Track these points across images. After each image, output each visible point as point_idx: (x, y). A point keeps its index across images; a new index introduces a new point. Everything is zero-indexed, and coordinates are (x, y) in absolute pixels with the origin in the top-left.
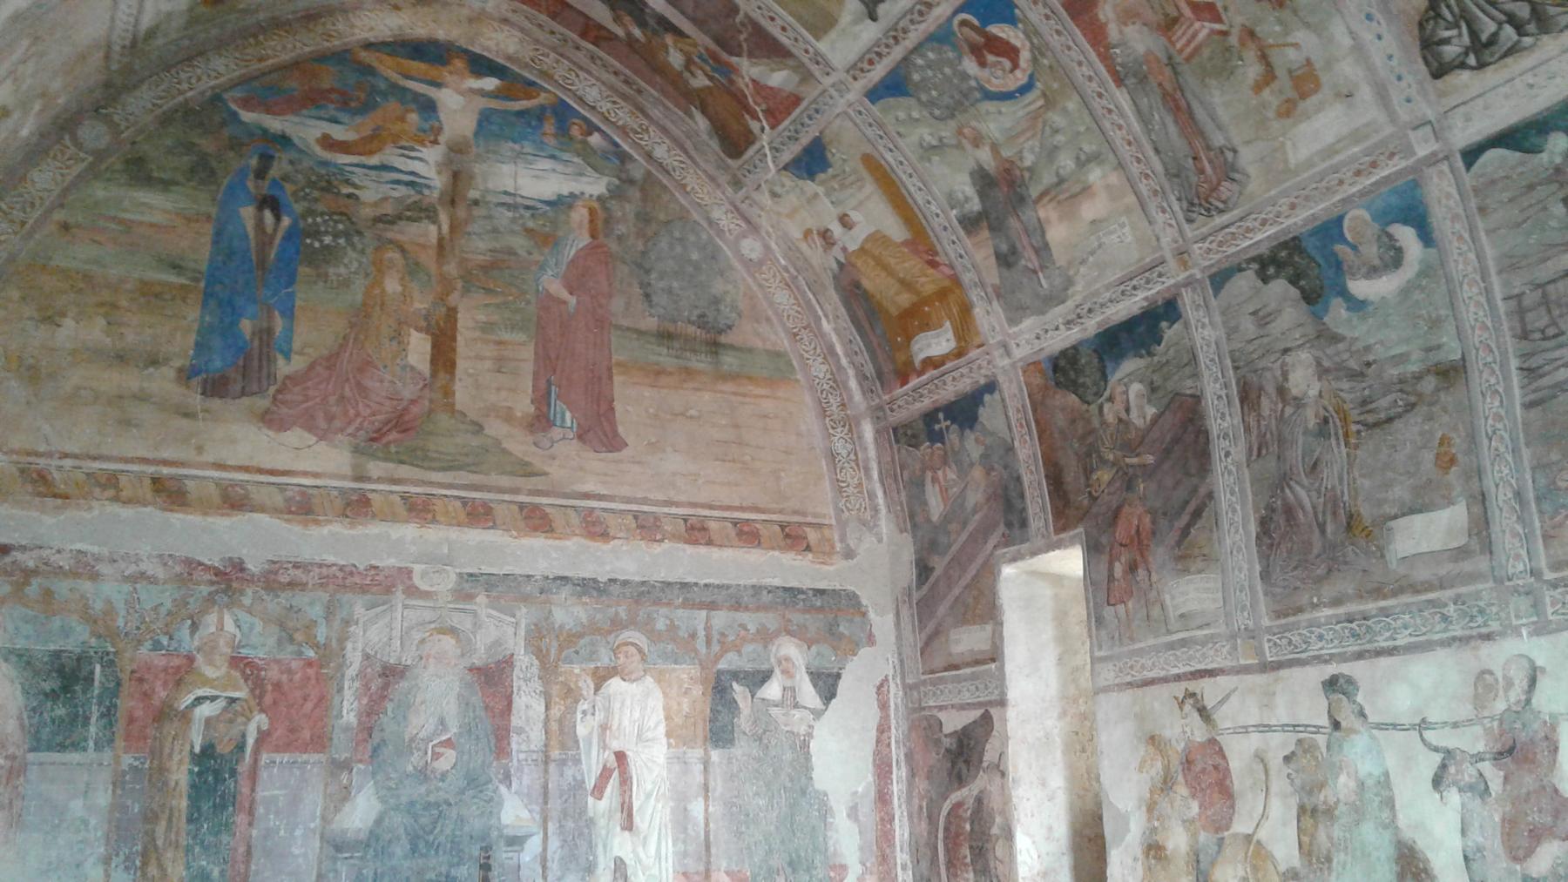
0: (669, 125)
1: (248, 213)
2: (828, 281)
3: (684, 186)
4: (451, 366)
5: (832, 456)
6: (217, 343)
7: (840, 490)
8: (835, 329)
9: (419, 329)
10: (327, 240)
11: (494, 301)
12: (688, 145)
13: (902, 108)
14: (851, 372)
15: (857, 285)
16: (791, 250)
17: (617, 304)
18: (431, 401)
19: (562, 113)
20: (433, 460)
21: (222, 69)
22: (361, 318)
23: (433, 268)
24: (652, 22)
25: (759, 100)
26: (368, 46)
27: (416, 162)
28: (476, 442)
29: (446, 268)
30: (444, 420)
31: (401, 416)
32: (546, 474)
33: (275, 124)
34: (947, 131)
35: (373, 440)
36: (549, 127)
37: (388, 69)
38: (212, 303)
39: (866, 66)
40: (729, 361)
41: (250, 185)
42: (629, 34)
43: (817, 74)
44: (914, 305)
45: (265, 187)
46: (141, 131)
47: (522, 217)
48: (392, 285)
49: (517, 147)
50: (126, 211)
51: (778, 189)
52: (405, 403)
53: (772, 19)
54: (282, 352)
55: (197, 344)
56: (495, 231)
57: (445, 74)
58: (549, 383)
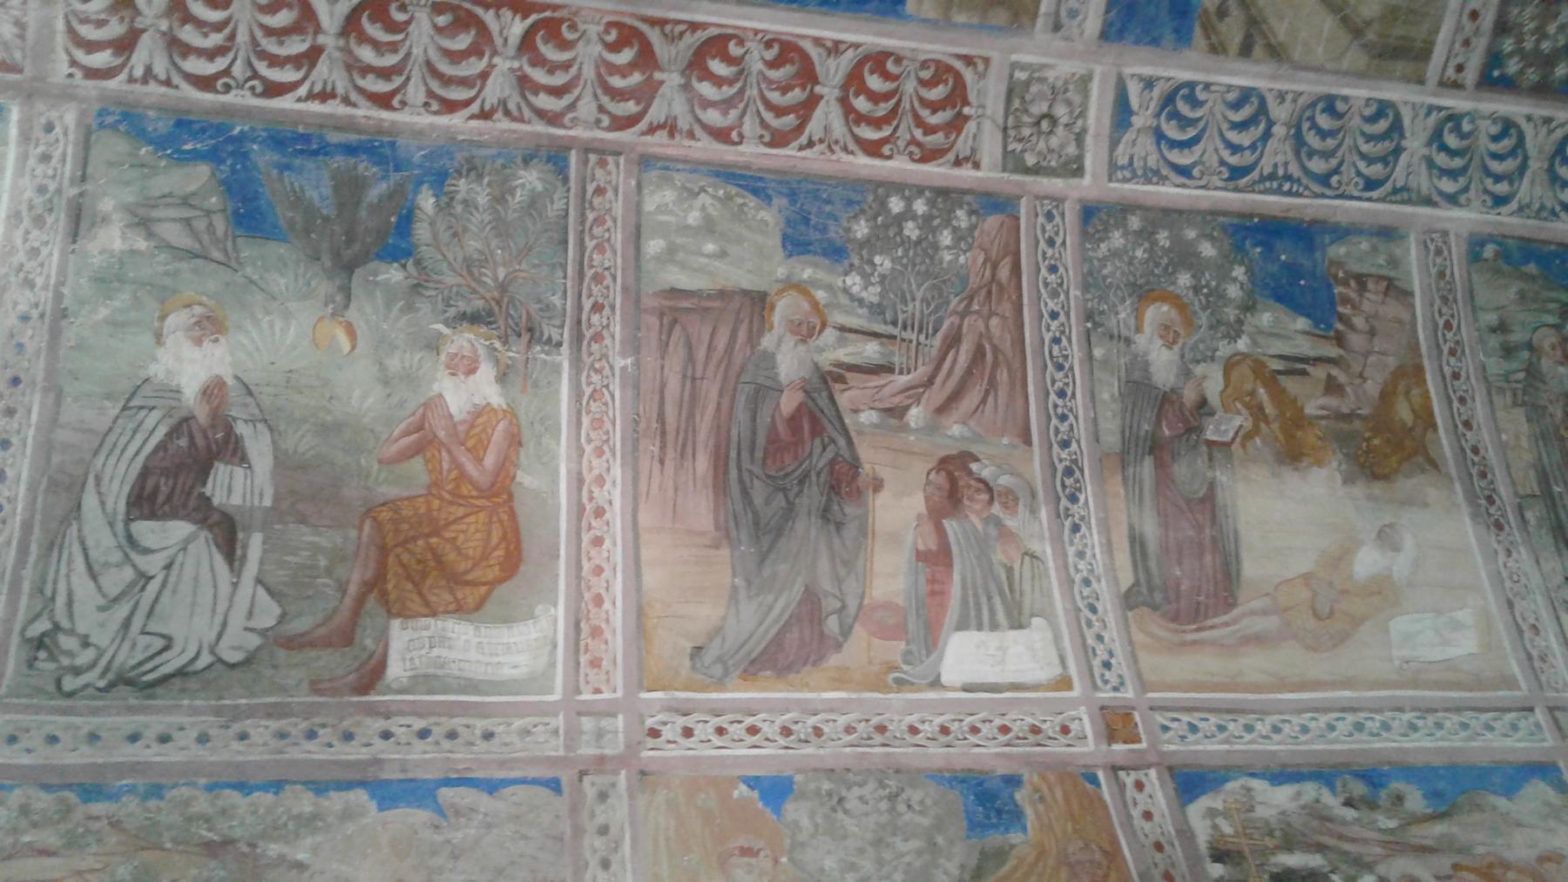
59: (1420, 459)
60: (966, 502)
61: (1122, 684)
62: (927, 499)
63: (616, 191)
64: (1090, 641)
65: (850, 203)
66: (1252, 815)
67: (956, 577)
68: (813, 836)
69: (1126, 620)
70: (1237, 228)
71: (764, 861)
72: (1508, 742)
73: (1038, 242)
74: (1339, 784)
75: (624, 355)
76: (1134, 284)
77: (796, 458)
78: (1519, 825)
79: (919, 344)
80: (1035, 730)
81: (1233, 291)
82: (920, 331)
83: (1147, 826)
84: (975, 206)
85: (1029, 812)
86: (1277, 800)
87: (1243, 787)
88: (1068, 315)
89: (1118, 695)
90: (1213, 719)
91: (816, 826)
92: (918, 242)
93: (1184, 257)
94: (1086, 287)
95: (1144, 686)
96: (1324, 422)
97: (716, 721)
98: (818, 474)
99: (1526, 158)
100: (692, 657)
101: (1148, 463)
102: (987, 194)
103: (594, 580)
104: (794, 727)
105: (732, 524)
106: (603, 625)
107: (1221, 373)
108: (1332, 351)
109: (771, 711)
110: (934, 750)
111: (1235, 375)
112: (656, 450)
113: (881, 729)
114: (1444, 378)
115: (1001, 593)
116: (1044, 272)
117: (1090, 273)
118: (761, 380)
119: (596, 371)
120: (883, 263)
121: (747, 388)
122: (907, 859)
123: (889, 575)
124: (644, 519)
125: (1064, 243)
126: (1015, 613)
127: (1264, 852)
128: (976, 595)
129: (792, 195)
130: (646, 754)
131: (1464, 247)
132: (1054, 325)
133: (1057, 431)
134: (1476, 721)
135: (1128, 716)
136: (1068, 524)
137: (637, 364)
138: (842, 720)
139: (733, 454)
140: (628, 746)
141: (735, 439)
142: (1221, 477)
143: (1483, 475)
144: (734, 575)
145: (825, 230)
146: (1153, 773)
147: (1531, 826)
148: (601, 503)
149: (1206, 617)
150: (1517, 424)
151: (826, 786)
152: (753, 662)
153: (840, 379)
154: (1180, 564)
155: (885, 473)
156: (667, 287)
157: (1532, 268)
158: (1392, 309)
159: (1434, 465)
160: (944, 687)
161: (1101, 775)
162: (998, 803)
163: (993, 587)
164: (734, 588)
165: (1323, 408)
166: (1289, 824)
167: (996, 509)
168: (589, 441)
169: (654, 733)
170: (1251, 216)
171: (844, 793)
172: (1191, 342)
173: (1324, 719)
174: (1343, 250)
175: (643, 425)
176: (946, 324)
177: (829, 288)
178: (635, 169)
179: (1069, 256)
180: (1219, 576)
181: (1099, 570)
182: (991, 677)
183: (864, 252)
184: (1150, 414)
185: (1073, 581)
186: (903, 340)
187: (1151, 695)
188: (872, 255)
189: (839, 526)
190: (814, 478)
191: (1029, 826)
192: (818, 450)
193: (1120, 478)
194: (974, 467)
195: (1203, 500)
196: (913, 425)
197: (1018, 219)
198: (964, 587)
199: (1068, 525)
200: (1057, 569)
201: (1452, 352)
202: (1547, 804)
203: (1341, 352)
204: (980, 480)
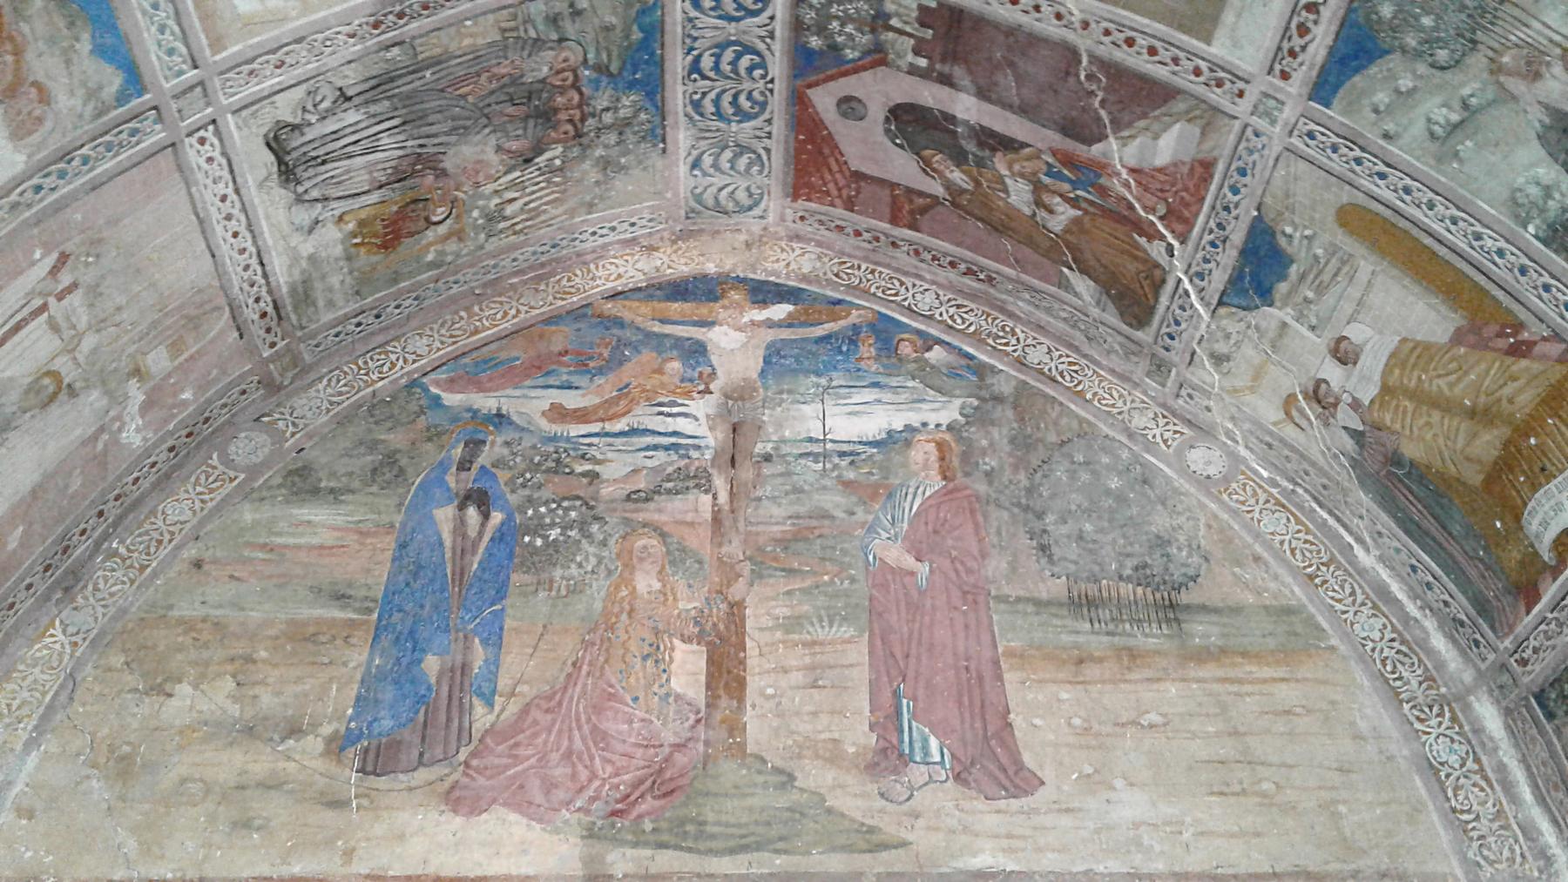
0: (1044, 317)
1: (444, 516)
2: (1345, 475)
3: (1081, 394)
4: (738, 687)
5: (1432, 770)
6: (388, 694)
7: (1464, 828)
8: (1381, 559)
9: (686, 639)
10: (554, 533)
11: (797, 584)
12: (1079, 338)
13: (1375, 85)
14: (1430, 624)
15: (1395, 459)
16: (1269, 445)
17: (996, 565)
18: (707, 743)
19: (884, 332)
20: (713, 837)
21: (423, 351)
22: (601, 634)
23: (707, 551)
24: (970, 146)
25: (1150, 200)
26: (615, 295)
27: (679, 419)
28: (783, 801)
29: (724, 550)
30: (729, 771)
31: (661, 771)
32: (904, 844)
33: (488, 403)
34: (1472, 83)
35: (614, 813)
36: (867, 349)
37: (639, 314)
38: (386, 640)
39: (1297, 42)
40: (1201, 630)
41: (451, 480)
42: (948, 186)
43: (1225, 104)
44: (1506, 445)
45: (469, 479)
46: (310, 436)
47: (836, 467)
48: (646, 582)
49: (823, 381)
50: (280, 534)
51: (1222, 348)
52: (667, 750)
53: (1130, 42)
54: (481, 695)
55: (358, 699)
56: (797, 490)
57: (719, 310)
58: (896, 694)
72: (153, 48)
78: (68, 62)
99: (738, 20)
157: (637, 35)
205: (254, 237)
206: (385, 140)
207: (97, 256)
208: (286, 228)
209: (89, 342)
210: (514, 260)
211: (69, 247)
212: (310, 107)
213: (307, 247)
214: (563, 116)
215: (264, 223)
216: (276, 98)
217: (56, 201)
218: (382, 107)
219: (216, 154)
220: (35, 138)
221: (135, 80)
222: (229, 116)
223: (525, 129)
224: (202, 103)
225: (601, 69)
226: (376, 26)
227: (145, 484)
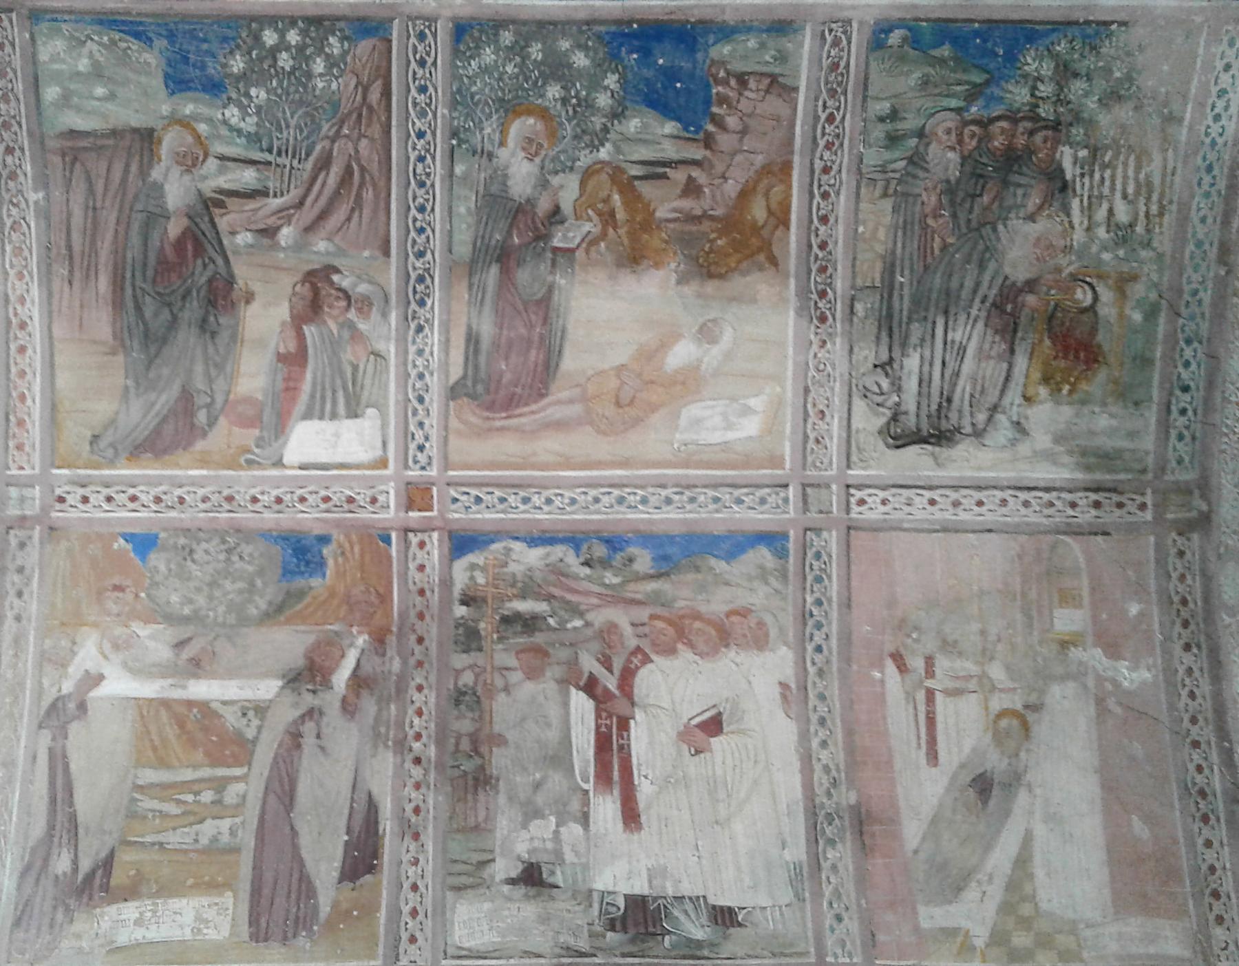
59: (761, 257)
60: (326, 309)
61: (429, 464)
62: (292, 308)
63: (13, 45)
64: (412, 428)
65: (225, 39)
66: (505, 570)
67: (309, 376)
68: (166, 578)
69: (447, 405)
70: (614, 35)
71: (129, 596)
73: (409, 62)
74: (585, 547)
75: (36, 190)
76: (502, 100)
77: (179, 277)
78: (727, 584)
79: (292, 168)
80: (351, 500)
81: (603, 100)
82: (294, 157)
83: (419, 576)
84: (347, 33)
85: (331, 562)
86: (529, 558)
87: (505, 548)
88: (434, 134)
89: (424, 473)
90: (498, 493)
91: (170, 570)
92: (294, 69)
93: (557, 69)
94: (453, 105)
95: (447, 465)
96: (671, 226)
97: (106, 491)
98: (198, 292)
100: (91, 443)
101: (494, 270)
102: (362, 20)
103: (19, 382)
104: (164, 497)
105: (126, 335)
106: (26, 418)
107: (578, 183)
108: (698, 153)
109: (149, 484)
110: (268, 515)
111: (591, 184)
112: (66, 273)
113: (230, 499)
114: (812, 171)
115: (345, 388)
116: (414, 92)
117: (459, 91)
118: (150, 209)
119: (14, 205)
120: (259, 94)
121: (139, 216)
122: (230, 597)
123: (253, 375)
124: (57, 332)
125: (435, 63)
126: (353, 403)
127: (502, 599)
128: (323, 389)
129: (171, 36)
130: (54, 515)
131: (867, 32)
132: (420, 144)
133: (414, 242)
134: (725, 495)
135: (429, 490)
136: (413, 326)
137: (47, 198)
138: (201, 492)
139: (128, 275)
140: (43, 509)
141: (129, 261)
142: (561, 281)
143: (823, 270)
144: (126, 378)
145: (203, 67)
146: (435, 535)
147: (738, 585)
148: (24, 318)
149: (517, 406)
150: (879, 217)
151: (182, 541)
152: (136, 448)
153: (220, 204)
154: (507, 358)
155: (256, 287)
156: (64, 128)
157: (945, 51)
158: (773, 104)
159: (773, 261)
160: (284, 466)
161: (394, 536)
162: (309, 556)
163: (339, 382)
164: (126, 388)
165: (675, 210)
166: (531, 578)
167: (352, 315)
168: (12, 266)
169: (61, 500)
170: (629, 23)
171: (194, 546)
172: (552, 153)
173: (593, 492)
174: (726, 49)
175: (54, 251)
176: (318, 148)
177: (210, 121)
178: (27, 23)
179: (439, 76)
180: (539, 369)
181: (434, 364)
182: (324, 458)
183: (241, 85)
184: (503, 225)
185: (409, 375)
186: (278, 165)
187: (451, 473)
188: (247, 87)
189: (213, 334)
190: (195, 294)
191: (328, 573)
192: (199, 269)
193: (465, 284)
194: (335, 278)
195: (538, 303)
196: (283, 243)
197: (390, 41)
198: (314, 384)
199: (414, 325)
200: (397, 366)
201: (829, 146)
202: (762, 567)
203: (708, 153)
204: (340, 289)
205: (995, 487)
206: (957, 335)
207: (916, 628)
208: (1006, 455)
209: (997, 672)
210: (1203, 220)
211: (889, 647)
212: (879, 399)
213: (1042, 440)
214: (1021, 141)
215: (983, 474)
216: (854, 427)
217: (839, 640)
218: (916, 330)
219: (882, 494)
220: (773, 632)
221: (772, 539)
222: (850, 472)
223: (1019, 185)
224: (824, 491)
225: (970, 98)
226: (823, 319)
227: (1205, 688)
